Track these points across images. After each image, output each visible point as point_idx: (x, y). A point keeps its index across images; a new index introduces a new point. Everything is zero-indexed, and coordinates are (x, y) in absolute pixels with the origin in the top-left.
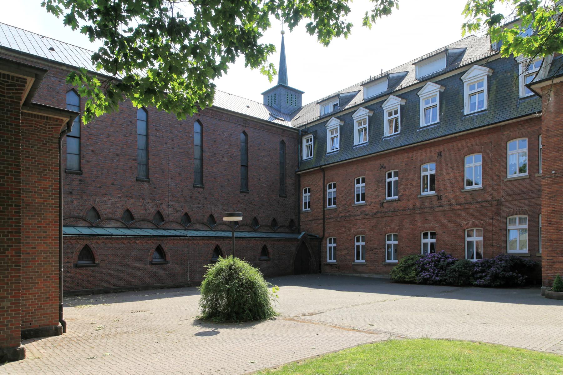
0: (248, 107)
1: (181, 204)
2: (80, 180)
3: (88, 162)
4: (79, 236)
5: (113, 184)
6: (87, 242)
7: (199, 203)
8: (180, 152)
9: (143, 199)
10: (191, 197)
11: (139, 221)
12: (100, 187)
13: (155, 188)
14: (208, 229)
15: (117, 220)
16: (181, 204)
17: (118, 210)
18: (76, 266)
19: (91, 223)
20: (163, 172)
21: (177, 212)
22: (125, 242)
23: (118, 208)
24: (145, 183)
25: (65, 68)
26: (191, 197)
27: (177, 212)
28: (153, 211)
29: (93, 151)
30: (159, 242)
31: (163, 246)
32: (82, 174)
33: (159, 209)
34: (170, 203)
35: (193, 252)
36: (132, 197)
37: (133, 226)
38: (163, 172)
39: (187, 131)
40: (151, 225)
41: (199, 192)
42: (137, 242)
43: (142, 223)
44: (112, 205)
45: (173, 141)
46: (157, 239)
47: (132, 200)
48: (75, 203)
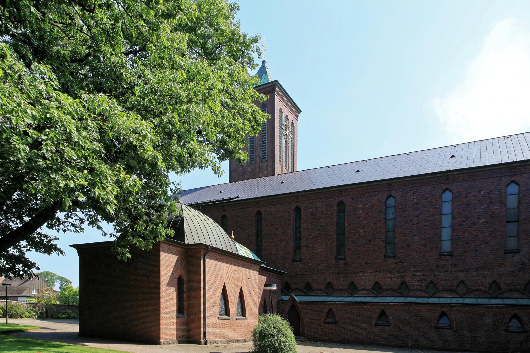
0: (358, 171)
1: (426, 273)
2: (344, 264)
3: (350, 249)
4: (325, 303)
5: (366, 263)
6: (331, 307)
7: (446, 271)
8: (425, 226)
9: (390, 272)
10: (437, 266)
11: (386, 291)
12: (357, 267)
13: (400, 262)
14: (399, 295)
15: (369, 291)
16: (426, 273)
17: (370, 283)
18: (324, 322)
19: (351, 294)
20: (408, 247)
21: (421, 281)
22: (356, 307)
23: (370, 281)
24: (392, 259)
25: (284, 196)
26: (437, 266)
27: (421, 281)
28: (399, 282)
29: (352, 241)
30: (382, 308)
31: (385, 311)
32: (345, 259)
33: (403, 280)
34: (415, 273)
35: (415, 317)
36: (380, 272)
37: (381, 295)
38: (408, 247)
39: (433, 204)
40: (396, 294)
41: (446, 260)
42: (364, 307)
43: (389, 292)
44: (365, 279)
45: (418, 216)
46: (381, 305)
47: (381, 274)
48: (341, 280)
